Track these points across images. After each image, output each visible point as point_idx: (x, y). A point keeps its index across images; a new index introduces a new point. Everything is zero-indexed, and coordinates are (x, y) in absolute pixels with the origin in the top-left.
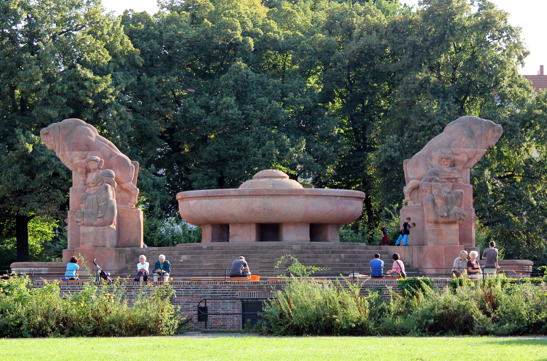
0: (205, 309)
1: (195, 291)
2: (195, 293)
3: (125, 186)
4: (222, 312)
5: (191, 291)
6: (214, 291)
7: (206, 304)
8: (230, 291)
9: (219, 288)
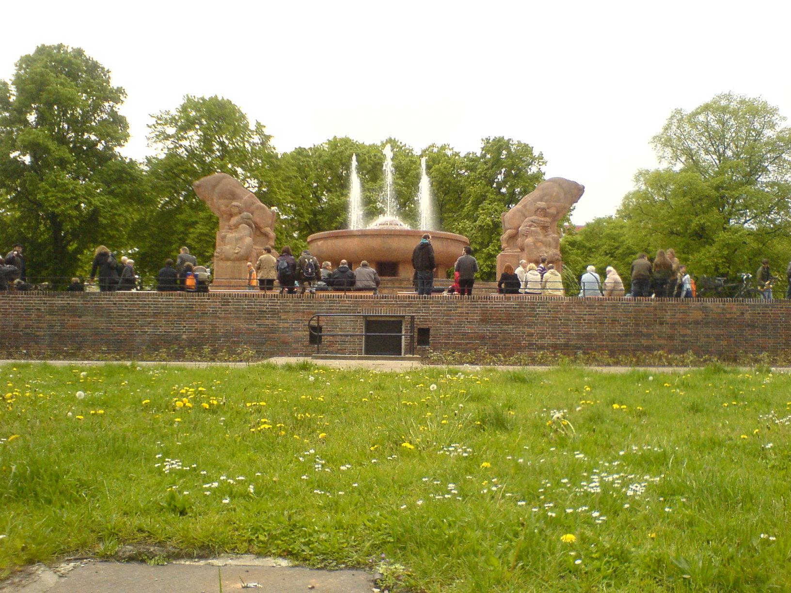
0: (319, 329)
1: (306, 306)
2: (306, 309)
3: (263, 230)
4: (340, 333)
5: (302, 306)
6: (330, 306)
7: (318, 323)
8: (350, 307)
9: (337, 303)
